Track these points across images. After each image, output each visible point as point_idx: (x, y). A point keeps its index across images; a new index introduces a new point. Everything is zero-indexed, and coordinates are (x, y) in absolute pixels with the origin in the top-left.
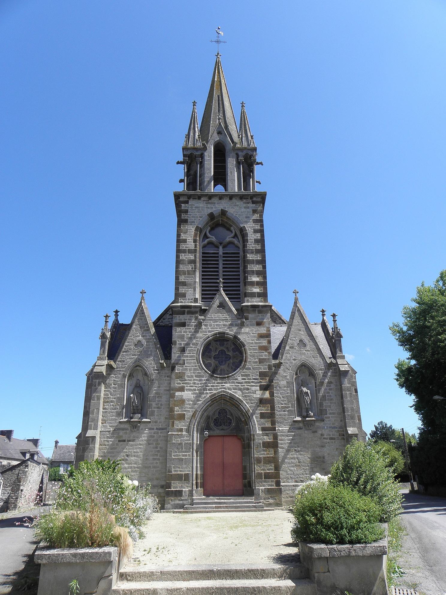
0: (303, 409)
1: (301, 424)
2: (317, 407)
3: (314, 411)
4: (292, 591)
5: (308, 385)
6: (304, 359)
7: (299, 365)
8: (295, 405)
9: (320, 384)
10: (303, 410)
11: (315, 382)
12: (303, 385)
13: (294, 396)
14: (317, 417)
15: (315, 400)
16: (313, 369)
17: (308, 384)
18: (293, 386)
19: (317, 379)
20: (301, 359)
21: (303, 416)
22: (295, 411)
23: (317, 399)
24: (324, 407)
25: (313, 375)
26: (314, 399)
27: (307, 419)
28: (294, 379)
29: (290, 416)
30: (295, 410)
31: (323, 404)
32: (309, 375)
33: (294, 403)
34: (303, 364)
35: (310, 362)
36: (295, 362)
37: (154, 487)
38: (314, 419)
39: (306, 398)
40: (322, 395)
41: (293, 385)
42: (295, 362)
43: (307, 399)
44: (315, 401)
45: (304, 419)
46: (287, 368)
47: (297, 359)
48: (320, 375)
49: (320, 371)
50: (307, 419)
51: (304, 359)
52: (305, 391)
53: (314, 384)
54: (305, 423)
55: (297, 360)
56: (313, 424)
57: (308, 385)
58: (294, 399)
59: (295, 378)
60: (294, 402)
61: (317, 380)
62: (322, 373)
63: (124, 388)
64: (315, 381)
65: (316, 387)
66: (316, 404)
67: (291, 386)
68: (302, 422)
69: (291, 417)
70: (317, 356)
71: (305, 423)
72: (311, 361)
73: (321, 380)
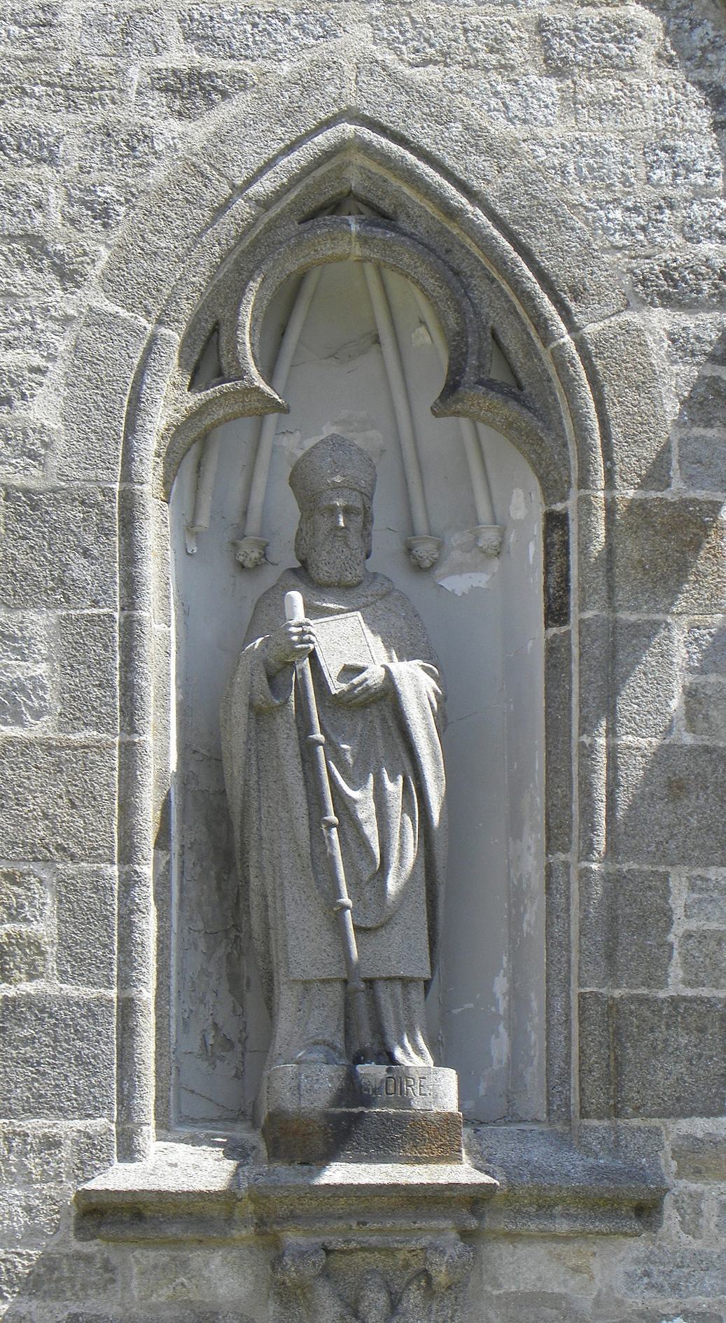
0: (287, 999)
1: (217, 1259)
2: (556, 980)
3: (500, 1047)
4: (136, 572)
5: (420, 568)
6: (377, 86)
7: (265, 186)
8: (127, 926)
9: (630, 549)
10: (284, 1025)
11: (556, 522)
12: (323, 571)
13: (130, 753)
14: (539, 1153)
15: (534, 838)
16: (516, 283)
17: (425, 550)
18: (131, 586)
19: (585, 449)
20: (307, 83)
21: (276, 1117)
22: (127, 1032)
23: (555, 837)
24: (676, 971)
25: (514, 391)
26: (515, 831)
27: (337, 1173)
28: (150, 446)
29: (35, 1126)
30: (127, 1008)
31: (666, 916)
32: (452, 388)
33: (129, 883)
34: (354, 180)
35: (477, 138)
36: (199, 131)
37: (604, 710)
38: (463, 1173)
39: (345, 807)
40: (664, 755)
41: (130, 557)
42: (199, 131)
43: (366, 811)
44: (532, 864)
45: (286, 1173)
46: (35, 243)
47: (241, 83)
48: (645, 383)
49: (659, 320)
50: (337, 1173)
51: (377, 86)
52: (350, 671)
53: (535, 551)
54: (293, 1238)
55: (239, 105)
56: (441, 1277)
57: (420, 568)
58: (128, 808)
59: (178, 431)
60: (128, 854)
61: (584, 483)
62: (680, 344)
63: (126, 982)
64: (552, 487)
65: (556, 613)
66: (534, 915)
67: (80, 569)
68: (244, 1233)
69: (51, 1143)
70: (625, 32)
71: (293, 1238)
72: (499, 127)
73: (656, 475)
